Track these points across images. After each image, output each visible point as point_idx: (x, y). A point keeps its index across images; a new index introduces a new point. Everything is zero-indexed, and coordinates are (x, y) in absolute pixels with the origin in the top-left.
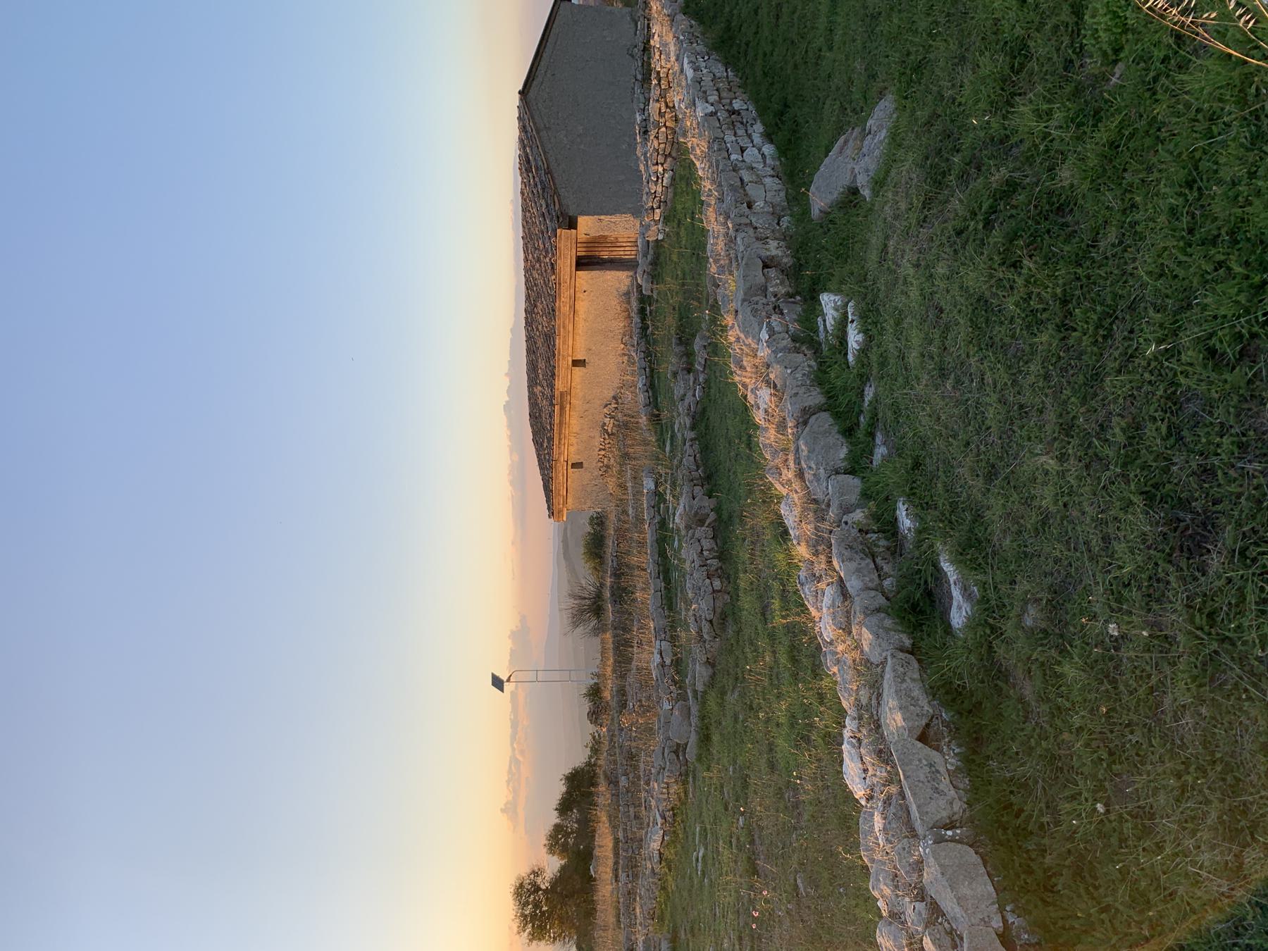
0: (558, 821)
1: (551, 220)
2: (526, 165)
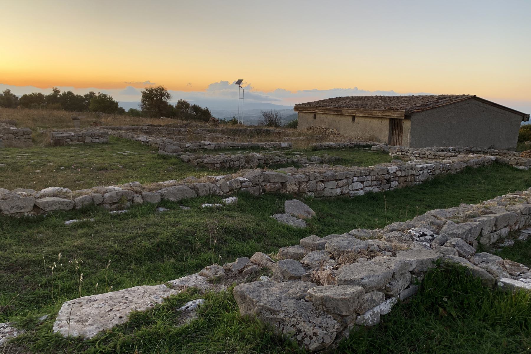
0: (191, 105)
1: (411, 108)
2: (442, 98)
